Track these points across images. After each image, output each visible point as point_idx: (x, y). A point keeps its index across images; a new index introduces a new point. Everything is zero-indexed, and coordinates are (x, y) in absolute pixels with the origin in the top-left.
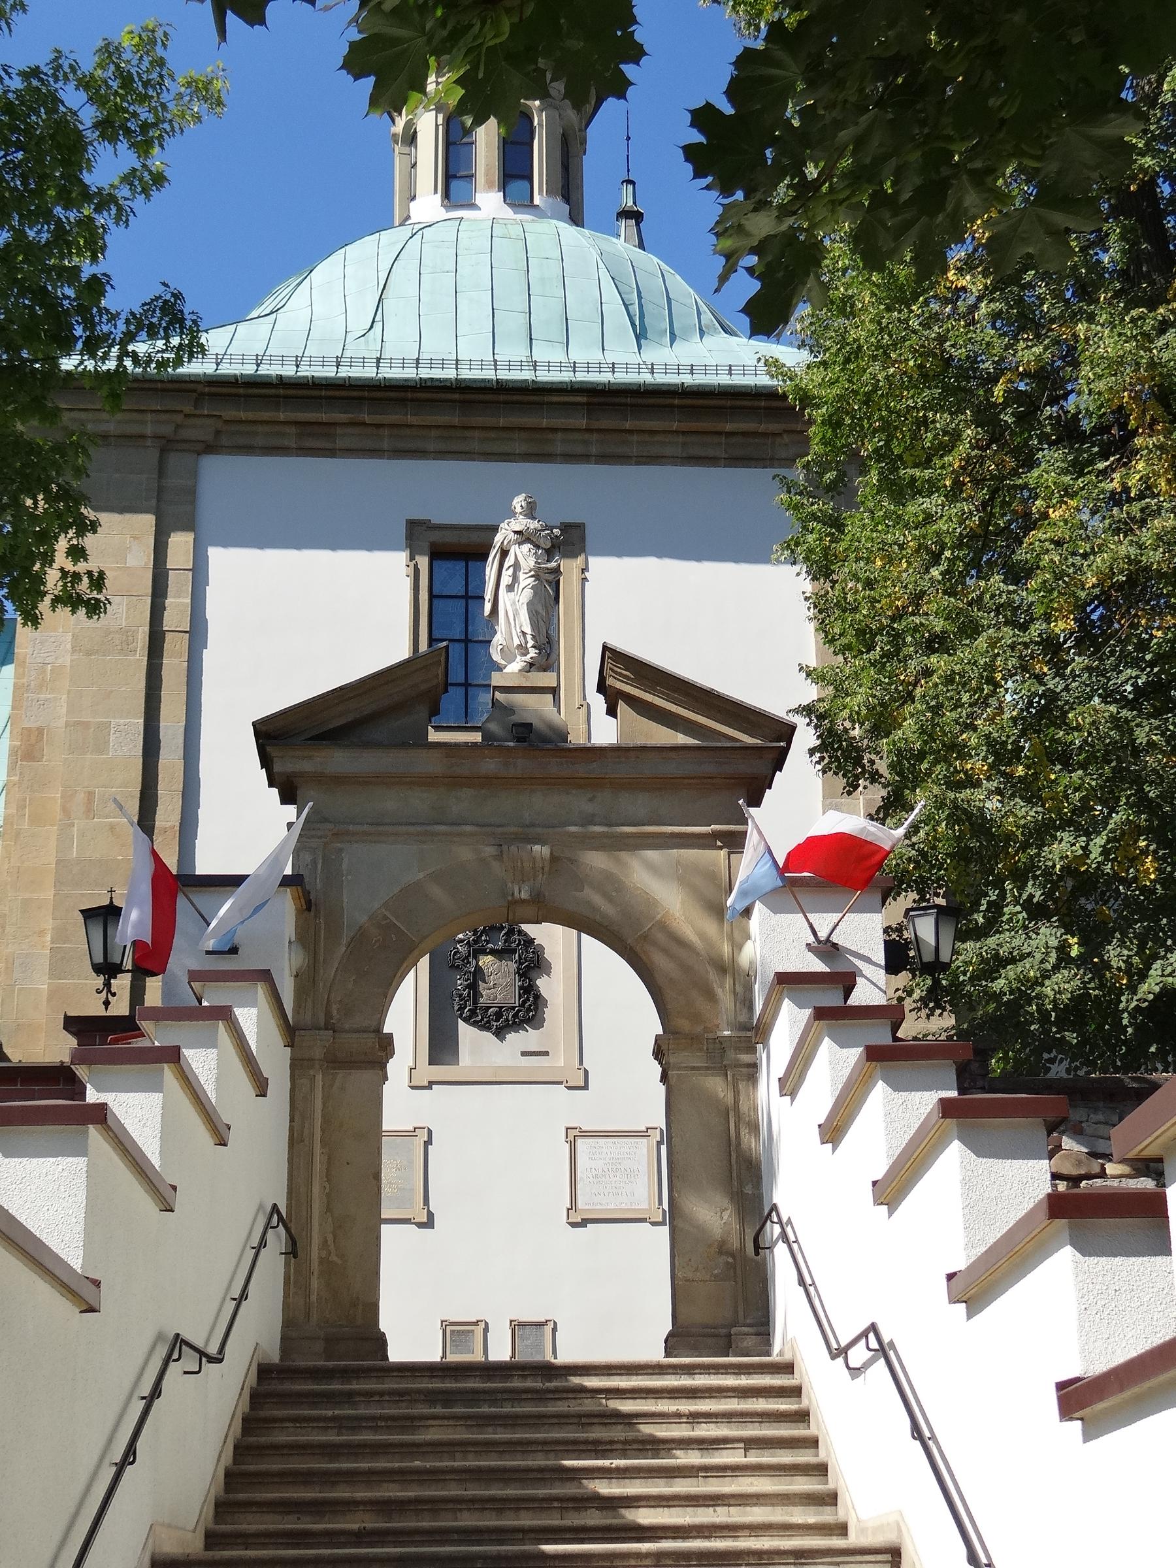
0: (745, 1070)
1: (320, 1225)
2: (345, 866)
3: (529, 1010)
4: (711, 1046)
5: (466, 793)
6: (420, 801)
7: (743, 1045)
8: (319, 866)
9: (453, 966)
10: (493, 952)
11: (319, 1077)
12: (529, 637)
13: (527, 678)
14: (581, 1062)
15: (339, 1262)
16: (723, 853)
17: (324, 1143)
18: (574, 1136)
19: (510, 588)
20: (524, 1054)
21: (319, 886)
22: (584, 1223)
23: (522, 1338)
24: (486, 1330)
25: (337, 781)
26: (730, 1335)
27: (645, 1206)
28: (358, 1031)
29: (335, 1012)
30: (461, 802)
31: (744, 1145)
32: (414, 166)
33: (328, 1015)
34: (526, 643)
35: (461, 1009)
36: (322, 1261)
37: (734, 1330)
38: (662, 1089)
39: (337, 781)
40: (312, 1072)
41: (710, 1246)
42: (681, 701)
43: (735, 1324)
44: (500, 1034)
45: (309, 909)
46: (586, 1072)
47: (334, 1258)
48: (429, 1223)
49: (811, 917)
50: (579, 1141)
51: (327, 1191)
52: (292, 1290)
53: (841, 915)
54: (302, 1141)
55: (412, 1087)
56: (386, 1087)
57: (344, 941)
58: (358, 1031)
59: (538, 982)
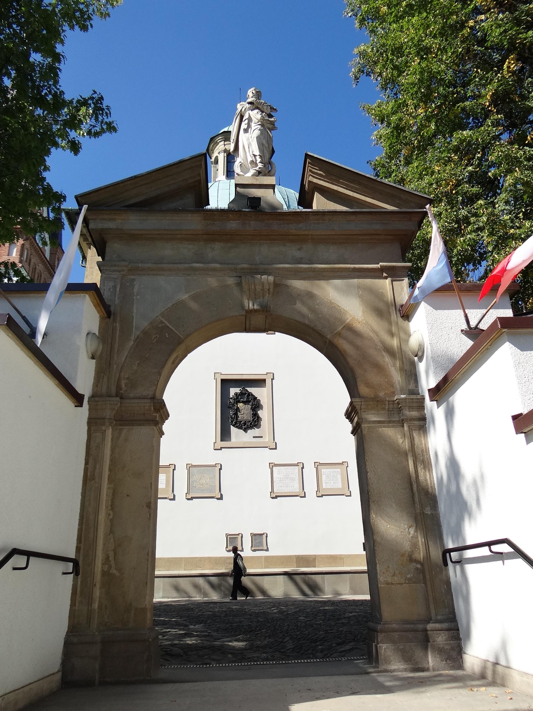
0: (417, 423)
1: (104, 544)
2: (135, 290)
3: (255, 422)
4: (391, 406)
5: (217, 246)
6: (187, 250)
7: (415, 405)
8: (118, 289)
9: (229, 407)
10: (243, 402)
11: (109, 432)
12: (258, 157)
13: (257, 180)
14: (274, 440)
15: (117, 574)
16: (388, 281)
17: (111, 480)
18: (272, 466)
19: (246, 131)
20: (254, 437)
21: (117, 302)
22: (276, 497)
23: (255, 540)
24: (242, 537)
25: (132, 237)
26: (426, 630)
27: (298, 491)
28: (139, 398)
29: (123, 386)
30: (215, 250)
31: (421, 478)
32: (217, 170)
33: (119, 387)
34: (256, 160)
35: (232, 422)
36: (104, 574)
37: (430, 626)
38: (352, 440)
39: (132, 237)
40: (103, 428)
41: (403, 555)
42: (356, 189)
43: (429, 620)
44: (245, 430)
45: (109, 316)
46: (276, 443)
47: (114, 571)
48: (221, 498)
49: (467, 311)
50: (274, 468)
51: (111, 517)
52: (78, 598)
53: (486, 310)
54: (94, 479)
55: (215, 449)
56: (163, 440)
57: (133, 338)
58: (139, 398)
59: (258, 412)
